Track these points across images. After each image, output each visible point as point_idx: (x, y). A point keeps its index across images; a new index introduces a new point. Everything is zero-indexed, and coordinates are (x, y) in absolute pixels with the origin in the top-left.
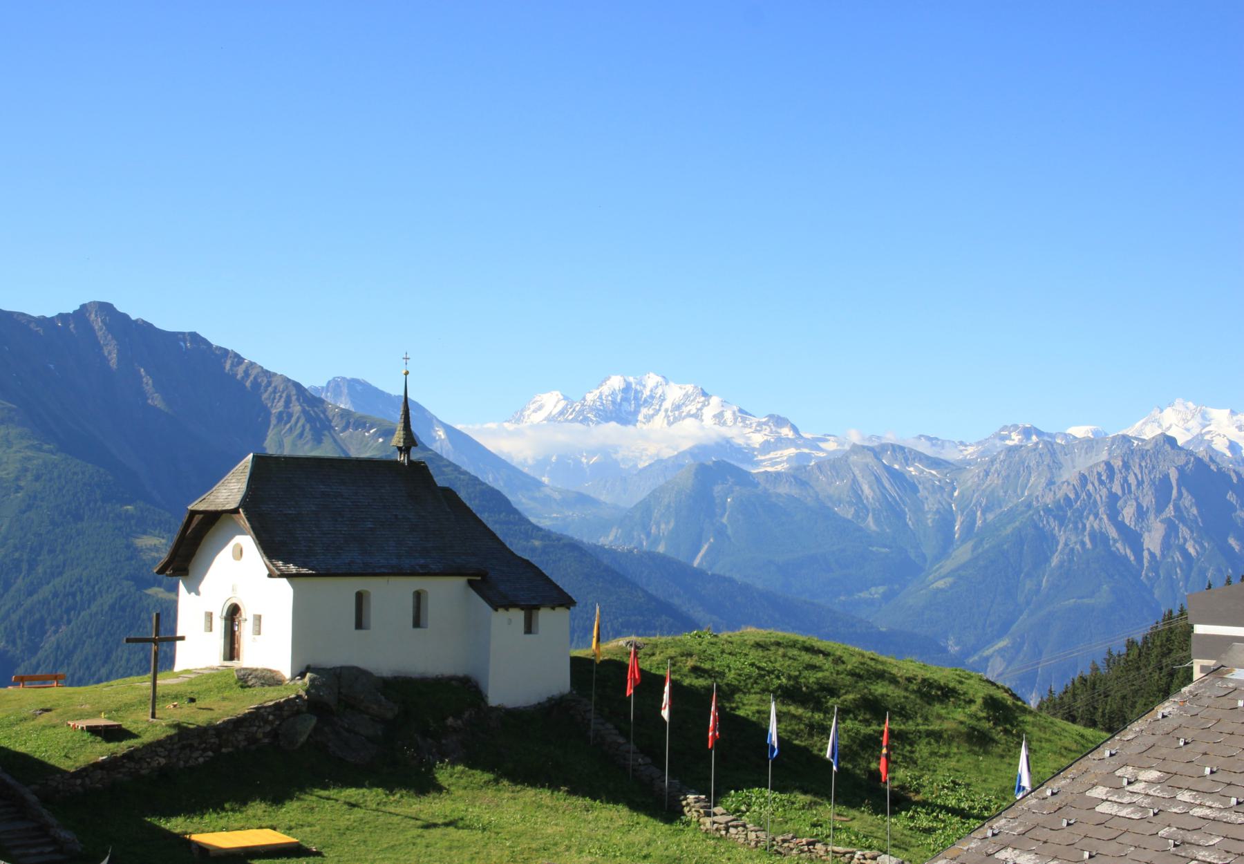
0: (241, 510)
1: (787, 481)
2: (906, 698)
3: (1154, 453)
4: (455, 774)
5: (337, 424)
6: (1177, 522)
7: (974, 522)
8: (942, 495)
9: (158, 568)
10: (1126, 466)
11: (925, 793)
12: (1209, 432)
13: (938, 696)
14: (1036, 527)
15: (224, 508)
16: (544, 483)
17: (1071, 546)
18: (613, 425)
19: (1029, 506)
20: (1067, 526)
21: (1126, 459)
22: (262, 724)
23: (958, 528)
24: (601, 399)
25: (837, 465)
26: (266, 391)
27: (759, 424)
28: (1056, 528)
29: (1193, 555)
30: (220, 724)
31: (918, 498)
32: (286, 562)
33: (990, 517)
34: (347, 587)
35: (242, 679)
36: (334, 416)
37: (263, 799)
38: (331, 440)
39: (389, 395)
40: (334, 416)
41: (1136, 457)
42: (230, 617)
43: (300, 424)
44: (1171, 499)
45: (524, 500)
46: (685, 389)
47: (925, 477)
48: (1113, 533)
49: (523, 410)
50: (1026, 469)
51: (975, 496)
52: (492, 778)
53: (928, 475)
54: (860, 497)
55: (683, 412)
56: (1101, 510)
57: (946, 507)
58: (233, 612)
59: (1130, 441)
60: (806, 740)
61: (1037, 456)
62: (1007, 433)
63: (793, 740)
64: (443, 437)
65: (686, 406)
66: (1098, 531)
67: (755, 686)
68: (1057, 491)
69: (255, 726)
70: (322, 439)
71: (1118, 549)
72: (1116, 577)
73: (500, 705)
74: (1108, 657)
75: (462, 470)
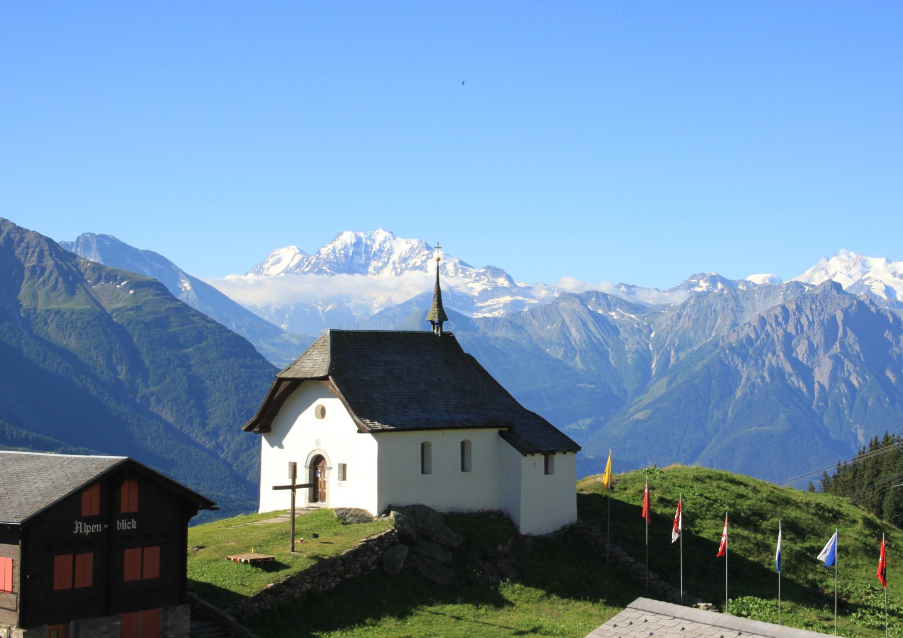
0: (330, 377)
1: (504, 325)
2: (812, 520)
3: (823, 296)
4: (516, 591)
5: (89, 277)
6: (842, 358)
7: (669, 360)
8: (640, 337)
9: (246, 427)
10: (799, 309)
11: (855, 598)
12: (869, 278)
13: (830, 517)
14: (722, 363)
15: (313, 376)
16: (283, 330)
17: (753, 380)
18: (345, 276)
19: (716, 345)
20: (749, 362)
21: (799, 303)
22: (371, 554)
23: (655, 366)
24: (335, 252)
25: (548, 311)
26: (19, 247)
27: (478, 275)
28: (740, 365)
29: (856, 387)
30: (344, 555)
31: (620, 339)
32: (372, 420)
33: (682, 355)
34: (417, 438)
35: (341, 518)
36: (86, 270)
37: (392, 615)
38: (84, 292)
39: (137, 250)
40: (86, 270)
41: (807, 301)
42: (313, 466)
43: (53, 277)
44: (837, 337)
45: (265, 346)
46: (411, 243)
47: (626, 321)
48: (788, 368)
49: (262, 263)
50: (713, 314)
51: (669, 336)
52: (545, 594)
53: (628, 319)
54: (568, 339)
55: (409, 264)
56: (778, 348)
57: (644, 347)
58: (317, 462)
59: (802, 287)
60: (757, 556)
61: (723, 301)
62: (696, 280)
63: (747, 556)
64: (189, 288)
65: (412, 259)
66: (775, 366)
67: (708, 512)
68: (740, 331)
69: (366, 556)
70: (75, 292)
71: (792, 382)
72: (791, 407)
73: (528, 534)
74: (824, 479)
75: (208, 319)
